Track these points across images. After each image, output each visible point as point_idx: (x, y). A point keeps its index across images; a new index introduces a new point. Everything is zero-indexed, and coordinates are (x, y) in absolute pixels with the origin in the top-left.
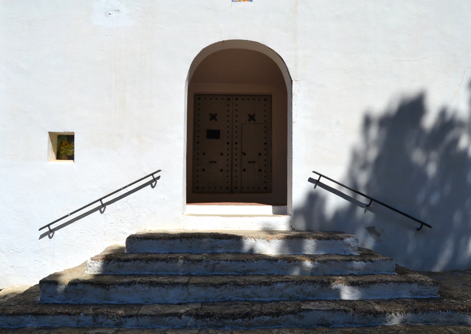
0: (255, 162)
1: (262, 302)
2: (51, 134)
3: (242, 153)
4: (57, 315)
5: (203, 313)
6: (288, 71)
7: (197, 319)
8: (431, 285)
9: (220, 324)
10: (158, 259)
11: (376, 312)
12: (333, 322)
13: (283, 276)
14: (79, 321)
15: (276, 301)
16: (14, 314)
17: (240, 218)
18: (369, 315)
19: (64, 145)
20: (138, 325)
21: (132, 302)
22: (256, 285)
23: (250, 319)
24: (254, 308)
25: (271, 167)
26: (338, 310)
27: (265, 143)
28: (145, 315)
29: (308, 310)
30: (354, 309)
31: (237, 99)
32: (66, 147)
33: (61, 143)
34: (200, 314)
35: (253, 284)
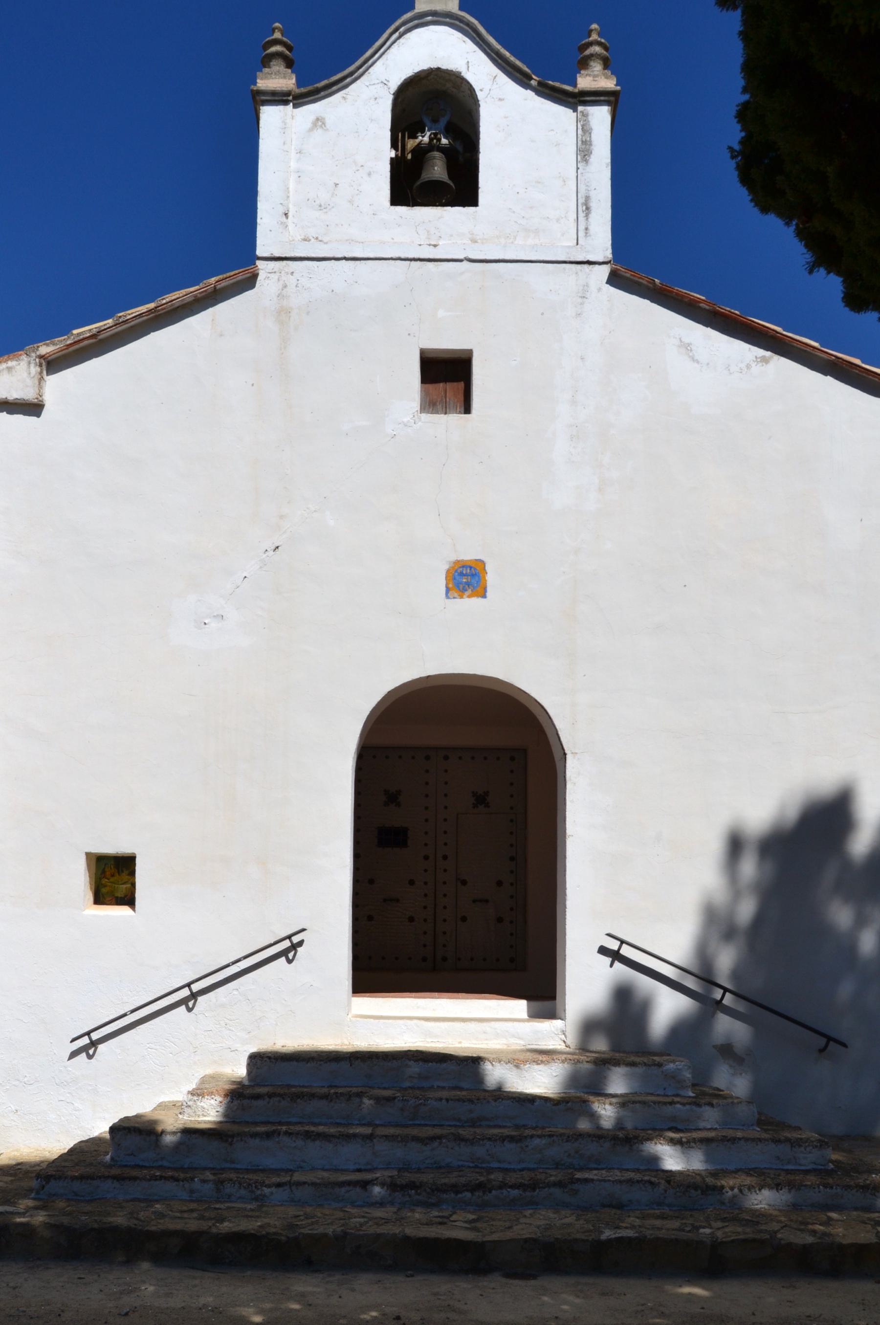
0: (487, 901)
1: (506, 1170)
2: (88, 855)
4: (156, 1180)
5: (404, 1182)
6: (558, 734)
8: (816, 1146)
10: (313, 1096)
11: (707, 1186)
12: (630, 1201)
13: (543, 1128)
14: (192, 1191)
15: (529, 1169)
17: (462, 1024)
18: (693, 1191)
19: (113, 879)
21: (273, 1167)
22: (496, 1140)
23: (484, 1193)
24: (492, 1177)
26: (638, 1182)
27: (512, 859)
28: (305, 1183)
29: (586, 1181)
30: (669, 1182)
32: (112, 880)
33: (104, 872)
34: (398, 1183)
35: (490, 1139)
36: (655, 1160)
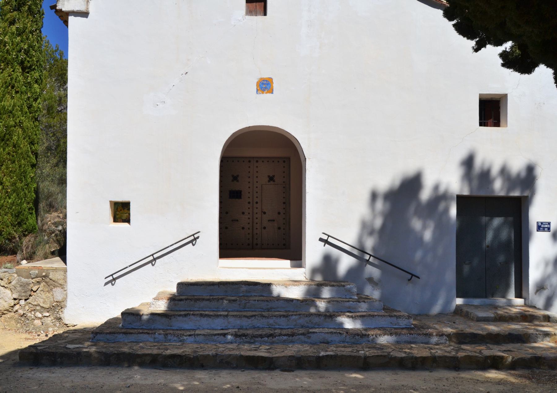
0: (274, 221)
1: (282, 329)
2: (111, 202)
3: (262, 212)
7: (236, 337)
9: (252, 341)
10: (203, 299)
14: (155, 338)
16: (110, 333)
20: (195, 342)
24: (276, 331)
25: (289, 225)
29: (314, 332)
30: (347, 333)
31: (257, 161)
33: (117, 209)
36: (341, 324)
